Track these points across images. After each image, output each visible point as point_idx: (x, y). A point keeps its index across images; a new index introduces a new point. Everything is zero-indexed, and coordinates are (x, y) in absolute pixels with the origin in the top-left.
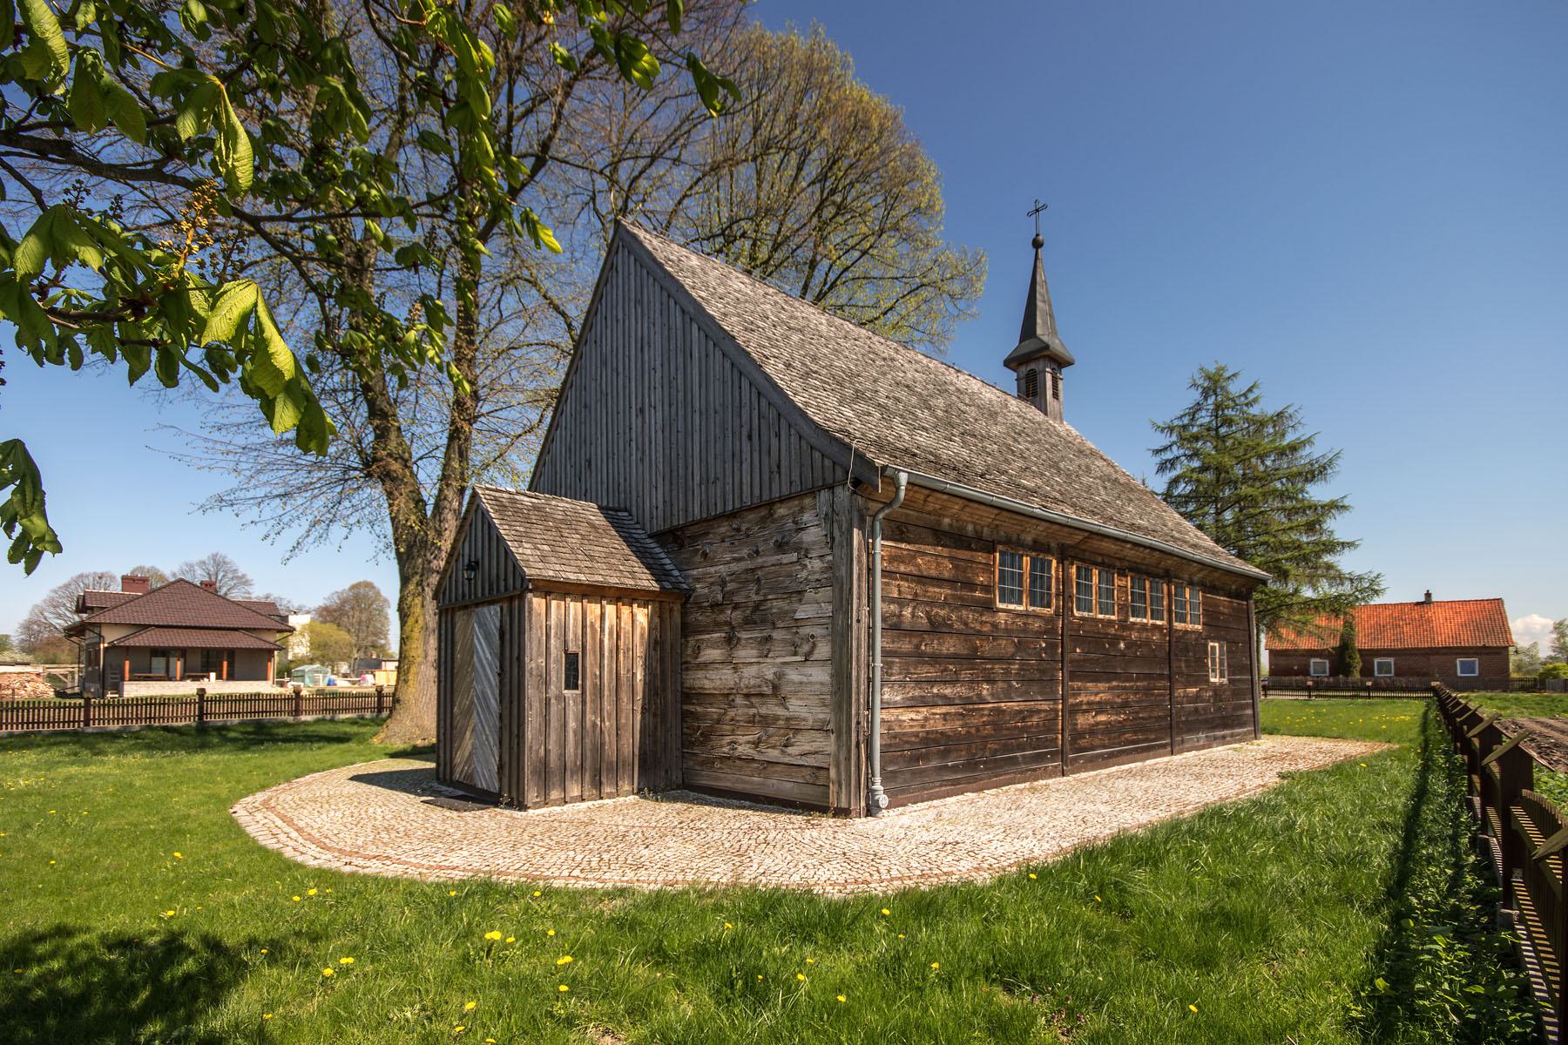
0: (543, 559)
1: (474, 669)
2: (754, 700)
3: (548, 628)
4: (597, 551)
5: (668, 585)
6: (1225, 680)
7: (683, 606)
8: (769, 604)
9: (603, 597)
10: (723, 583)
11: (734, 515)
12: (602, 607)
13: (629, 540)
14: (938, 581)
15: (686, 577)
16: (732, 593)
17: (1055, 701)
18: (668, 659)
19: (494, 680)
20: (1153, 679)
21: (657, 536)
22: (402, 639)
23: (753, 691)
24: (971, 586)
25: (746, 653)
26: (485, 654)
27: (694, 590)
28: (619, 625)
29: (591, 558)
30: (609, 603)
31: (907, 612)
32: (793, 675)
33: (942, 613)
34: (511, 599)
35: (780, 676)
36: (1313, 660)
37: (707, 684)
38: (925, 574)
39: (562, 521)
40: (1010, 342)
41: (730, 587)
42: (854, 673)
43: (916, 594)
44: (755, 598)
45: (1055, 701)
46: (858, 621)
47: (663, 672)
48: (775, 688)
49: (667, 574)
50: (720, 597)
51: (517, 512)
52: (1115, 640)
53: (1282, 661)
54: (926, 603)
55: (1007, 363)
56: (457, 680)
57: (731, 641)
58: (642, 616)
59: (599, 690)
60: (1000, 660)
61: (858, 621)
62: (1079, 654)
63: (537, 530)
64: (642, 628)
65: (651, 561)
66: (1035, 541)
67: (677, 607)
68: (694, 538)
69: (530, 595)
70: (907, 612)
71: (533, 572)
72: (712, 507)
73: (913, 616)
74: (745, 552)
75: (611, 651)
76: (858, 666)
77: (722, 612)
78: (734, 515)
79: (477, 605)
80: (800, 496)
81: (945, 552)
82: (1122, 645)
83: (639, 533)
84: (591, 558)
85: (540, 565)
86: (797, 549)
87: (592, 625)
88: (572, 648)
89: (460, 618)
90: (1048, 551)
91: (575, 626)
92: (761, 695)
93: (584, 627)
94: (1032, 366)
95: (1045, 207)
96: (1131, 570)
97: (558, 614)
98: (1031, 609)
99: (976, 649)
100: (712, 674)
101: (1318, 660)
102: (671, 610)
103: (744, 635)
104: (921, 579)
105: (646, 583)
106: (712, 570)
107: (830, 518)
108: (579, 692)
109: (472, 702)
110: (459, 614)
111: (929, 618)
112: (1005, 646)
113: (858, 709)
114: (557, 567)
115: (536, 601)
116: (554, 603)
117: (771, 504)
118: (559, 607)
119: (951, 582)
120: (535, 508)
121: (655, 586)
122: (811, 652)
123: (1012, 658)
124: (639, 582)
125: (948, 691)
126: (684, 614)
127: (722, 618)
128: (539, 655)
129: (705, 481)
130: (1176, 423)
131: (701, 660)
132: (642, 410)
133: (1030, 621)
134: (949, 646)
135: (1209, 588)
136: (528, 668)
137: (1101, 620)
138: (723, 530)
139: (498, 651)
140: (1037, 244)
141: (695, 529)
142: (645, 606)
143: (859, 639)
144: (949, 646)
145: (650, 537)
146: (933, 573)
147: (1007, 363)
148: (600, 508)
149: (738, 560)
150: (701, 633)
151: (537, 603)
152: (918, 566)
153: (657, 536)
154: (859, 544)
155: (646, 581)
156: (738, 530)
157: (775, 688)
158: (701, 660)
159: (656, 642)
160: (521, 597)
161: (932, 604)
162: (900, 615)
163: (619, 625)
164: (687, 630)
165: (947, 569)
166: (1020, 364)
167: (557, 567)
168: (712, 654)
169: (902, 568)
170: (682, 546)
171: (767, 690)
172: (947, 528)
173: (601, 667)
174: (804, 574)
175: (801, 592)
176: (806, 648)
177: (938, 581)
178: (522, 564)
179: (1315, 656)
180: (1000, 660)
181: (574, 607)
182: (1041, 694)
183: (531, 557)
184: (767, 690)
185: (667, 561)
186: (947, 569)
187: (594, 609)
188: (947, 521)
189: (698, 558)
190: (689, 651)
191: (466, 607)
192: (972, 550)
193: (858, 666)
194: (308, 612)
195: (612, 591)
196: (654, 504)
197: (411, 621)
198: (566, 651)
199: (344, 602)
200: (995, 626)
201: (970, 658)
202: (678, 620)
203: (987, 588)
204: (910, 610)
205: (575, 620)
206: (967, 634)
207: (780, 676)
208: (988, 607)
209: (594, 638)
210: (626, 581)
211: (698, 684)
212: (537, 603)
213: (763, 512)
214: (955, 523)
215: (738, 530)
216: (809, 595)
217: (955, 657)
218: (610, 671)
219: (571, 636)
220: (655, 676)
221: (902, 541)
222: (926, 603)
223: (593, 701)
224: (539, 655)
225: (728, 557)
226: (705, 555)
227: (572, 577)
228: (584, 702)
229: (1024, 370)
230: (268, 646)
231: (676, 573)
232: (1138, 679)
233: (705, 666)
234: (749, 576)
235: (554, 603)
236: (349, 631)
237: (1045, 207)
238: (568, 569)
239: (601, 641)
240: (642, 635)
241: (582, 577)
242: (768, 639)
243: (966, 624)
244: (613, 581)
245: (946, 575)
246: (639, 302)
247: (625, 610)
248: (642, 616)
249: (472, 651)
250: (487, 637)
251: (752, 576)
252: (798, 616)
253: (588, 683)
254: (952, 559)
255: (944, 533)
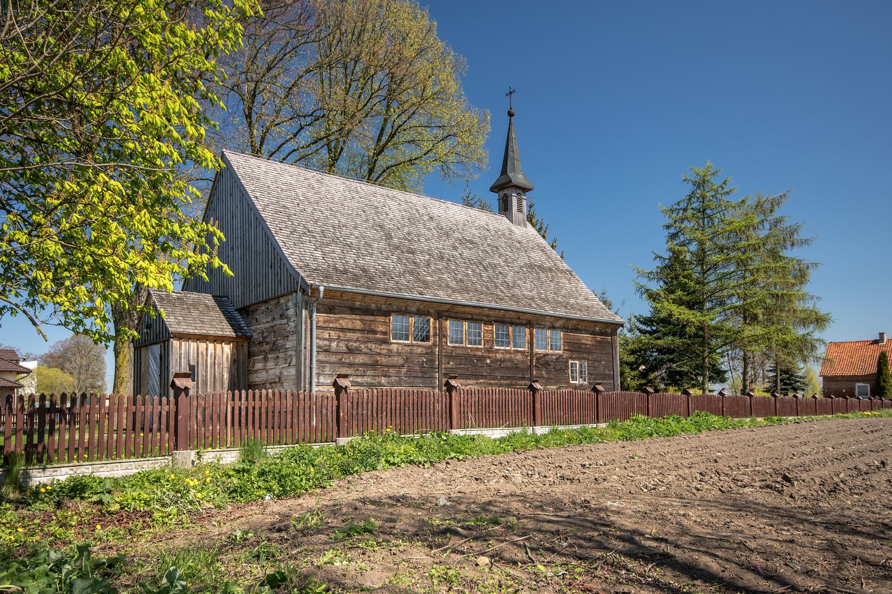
0: (179, 323)
1: (149, 375)
2: (273, 385)
3: (180, 354)
4: (206, 319)
5: (240, 334)
6: (586, 383)
7: (249, 343)
8: (278, 342)
9: (207, 340)
10: (263, 333)
11: (266, 302)
12: (215, 347)
13: (226, 313)
14: (353, 330)
15: (250, 330)
16: (266, 337)
17: (433, 387)
18: (241, 369)
19: (158, 378)
20: (516, 379)
21: (240, 310)
22: (116, 367)
23: (273, 381)
24: (374, 332)
25: (270, 364)
26: (154, 367)
27: (252, 336)
28: (215, 352)
29: (202, 322)
30: (211, 342)
31: (334, 344)
32: (285, 373)
33: (355, 345)
34: (164, 341)
35: (281, 373)
36: (858, 384)
37: (257, 380)
38: (345, 327)
39: (191, 305)
40: (494, 177)
41: (265, 334)
42: (303, 370)
43: (339, 336)
44: (274, 339)
45: (433, 387)
46: (305, 348)
47: (238, 374)
48: (280, 379)
49: (241, 328)
50: (261, 339)
51: (169, 301)
52: (482, 359)
53: (834, 386)
54: (346, 340)
55: (492, 189)
56: (142, 381)
57: (266, 359)
58: (227, 349)
59: (205, 383)
60: (394, 366)
61: (305, 348)
62: (452, 365)
63: (177, 310)
64: (227, 354)
65: (234, 323)
66: (418, 310)
67: (246, 344)
68: (253, 312)
69: (172, 340)
70: (334, 344)
71: (173, 329)
72: (270, 295)
73: (337, 346)
74: (270, 319)
75: (211, 365)
76: (305, 367)
77: (262, 346)
78: (266, 302)
79: (151, 345)
80: (287, 295)
81: (358, 317)
82: (488, 361)
83: (231, 309)
84: (202, 322)
85: (177, 326)
86: (287, 318)
87: (202, 353)
88: (192, 363)
89: (144, 351)
90: (428, 314)
91: (194, 353)
92: (275, 382)
93: (198, 354)
94: (506, 192)
95: (514, 91)
96: (496, 321)
97: (185, 348)
98: (414, 342)
99: (377, 361)
100: (259, 375)
101: (861, 384)
102: (243, 346)
103: (270, 356)
104: (343, 330)
105: (228, 333)
106: (259, 326)
107: (296, 305)
108: (195, 383)
109: (149, 390)
110: (143, 349)
111: (347, 347)
112: (396, 360)
113: (305, 384)
114: (185, 327)
115: (174, 342)
116: (183, 343)
117: (278, 298)
118: (185, 345)
119: (362, 331)
120: (179, 299)
121: (234, 334)
122: (290, 362)
123: (403, 366)
124: (225, 333)
125: (359, 380)
126: (249, 347)
127: (262, 349)
128: (176, 366)
129: (256, 285)
130: (675, 207)
131: (255, 368)
132: (233, 248)
133: (415, 348)
134: (360, 359)
135: (564, 328)
136: (171, 371)
137: (469, 348)
138: (263, 308)
139: (159, 365)
140: (511, 115)
141: (253, 307)
142: (229, 344)
143: (305, 356)
144: (360, 359)
145: (236, 310)
146: (350, 326)
147: (492, 189)
148: (213, 297)
149: (268, 322)
150: (255, 356)
151: (175, 343)
152: (341, 324)
153: (240, 310)
154: (306, 316)
155: (229, 332)
156: (268, 308)
157: (280, 379)
158: (255, 368)
159: (235, 361)
160: (168, 340)
161: (348, 341)
162: (330, 346)
163: (215, 352)
164: (250, 355)
165: (358, 325)
166: (500, 190)
167: (185, 327)
168: (259, 366)
169: (331, 325)
170: (248, 315)
171: (277, 380)
172: (358, 307)
173: (206, 372)
174: (288, 329)
175: (288, 336)
176: (289, 360)
177: (353, 330)
178: (168, 326)
179: (859, 381)
180: (394, 366)
181: (193, 345)
182: (422, 383)
183: (173, 323)
184: (277, 380)
185: (243, 322)
186: (358, 325)
187: (202, 346)
188: (358, 303)
189: (254, 321)
190: (251, 365)
191: (146, 346)
192: (374, 315)
193: (305, 367)
194: (34, 359)
195: (211, 338)
196: (238, 297)
197: (121, 356)
198: (189, 365)
199: (66, 350)
200: (390, 351)
201: (374, 365)
202: (247, 351)
203: (385, 333)
204: (335, 343)
205: (194, 350)
206: (370, 353)
207: (281, 373)
208: (386, 342)
209: (203, 359)
210: (218, 332)
211: (254, 380)
212: (175, 343)
213: (276, 301)
214: (363, 304)
215: (268, 308)
216: (290, 338)
217: (363, 365)
218: (211, 374)
219: (191, 358)
220: (234, 376)
221: (331, 313)
222: (346, 340)
223: (202, 387)
224: (176, 366)
225: (264, 321)
226: (257, 320)
227: (191, 331)
228: (198, 387)
229: (502, 193)
230: (10, 384)
231: (246, 328)
232: (501, 379)
233: (256, 371)
234: (272, 330)
235: (183, 343)
236: (71, 373)
237: (514, 91)
238: (190, 327)
239: (206, 360)
240: (227, 358)
241: (196, 331)
242: (278, 357)
243: (371, 350)
244: (212, 333)
245: (358, 328)
246: (231, 194)
247: (218, 346)
248: (227, 349)
249: (148, 366)
250: (155, 359)
251: (272, 330)
252: (287, 347)
253: (200, 379)
254: (361, 320)
255: (357, 309)
